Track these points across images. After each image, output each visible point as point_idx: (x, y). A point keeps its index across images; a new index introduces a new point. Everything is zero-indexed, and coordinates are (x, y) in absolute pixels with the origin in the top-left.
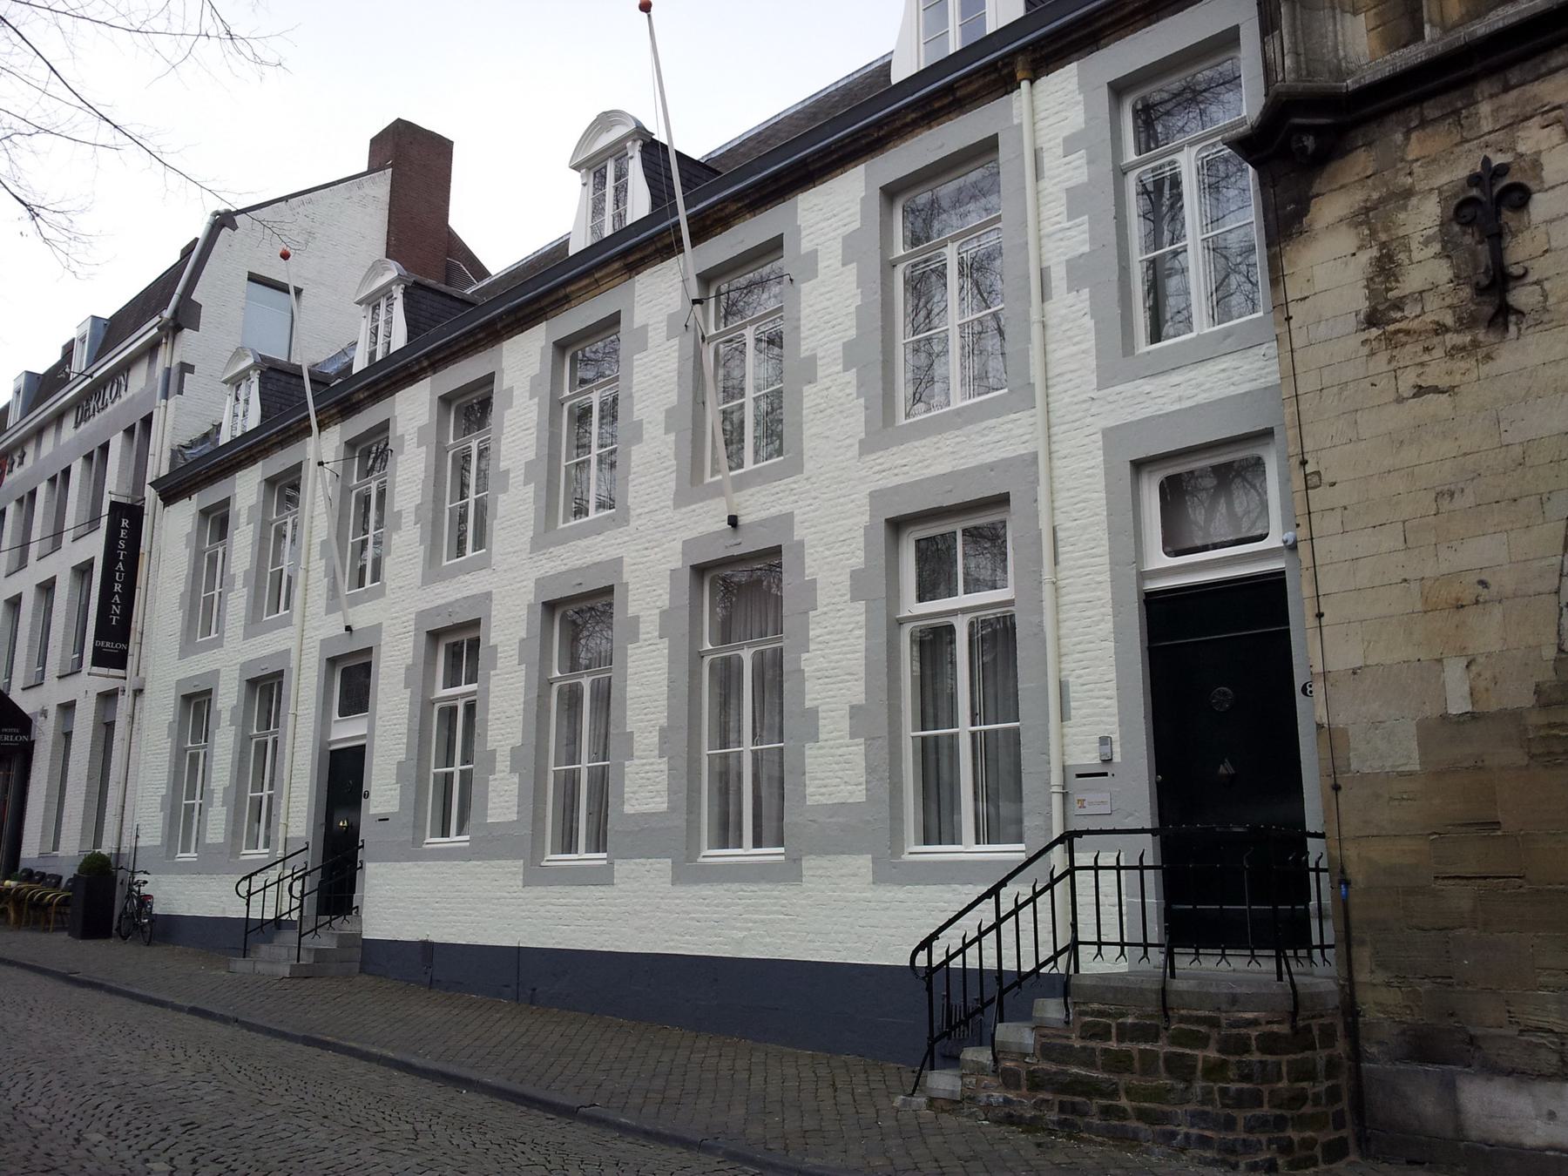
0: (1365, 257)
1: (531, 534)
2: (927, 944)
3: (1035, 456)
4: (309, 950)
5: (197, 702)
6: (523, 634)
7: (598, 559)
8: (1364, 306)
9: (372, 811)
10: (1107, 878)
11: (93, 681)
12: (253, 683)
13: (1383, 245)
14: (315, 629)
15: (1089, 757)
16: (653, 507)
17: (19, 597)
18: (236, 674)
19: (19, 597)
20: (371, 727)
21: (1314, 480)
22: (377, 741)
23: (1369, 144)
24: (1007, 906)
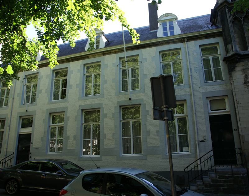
0: (244, 75)
2: (187, 167)
8: (244, 81)
9: (34, 146)
13: (246, 74)
20: (33, 130)
21: (238, 103)
22: (35, 133)
23: (243, 62)
24: (202, 160)
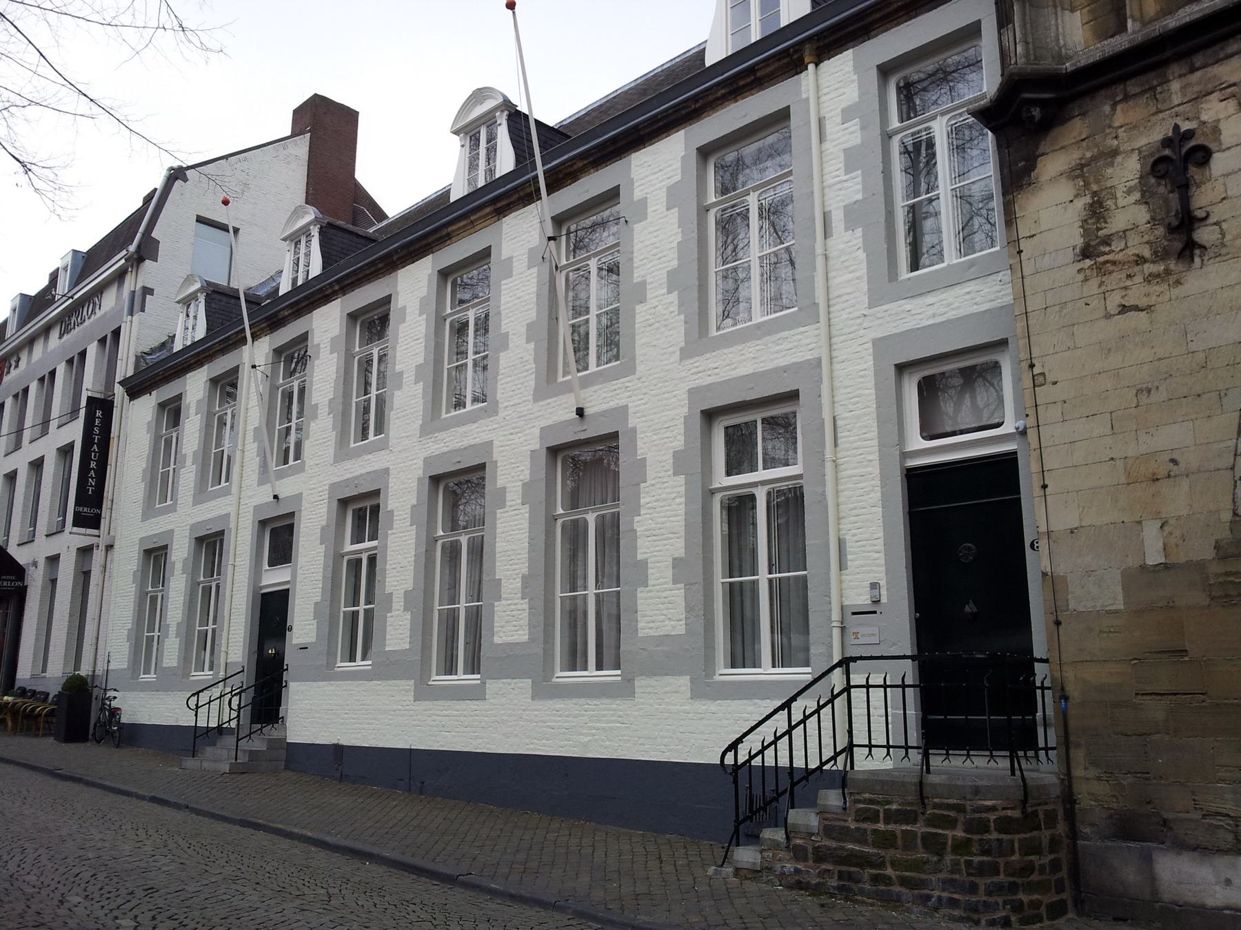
0: (1081, 203)
1: (420, 422)
2: (733, 747)
3: (819, 360)
4: (245, 751)
5: (156, 556)
6: (414, 502)
7: (473, 442)
8: (1079, 242)
9: (295, 641)
10: (876, 694)
11: (73, 538)
12: (200, 540)
13: (1095, 194)
14: (250, 497)
15: (862, 599)
16: (517, 401)
17: (15, 473)
18: (187, 533)
19: (15, 473)
20: (294, 575)
21: (1040, 380)
22: (298, 586)
23: (1083, 114)
24: (797, 716)
